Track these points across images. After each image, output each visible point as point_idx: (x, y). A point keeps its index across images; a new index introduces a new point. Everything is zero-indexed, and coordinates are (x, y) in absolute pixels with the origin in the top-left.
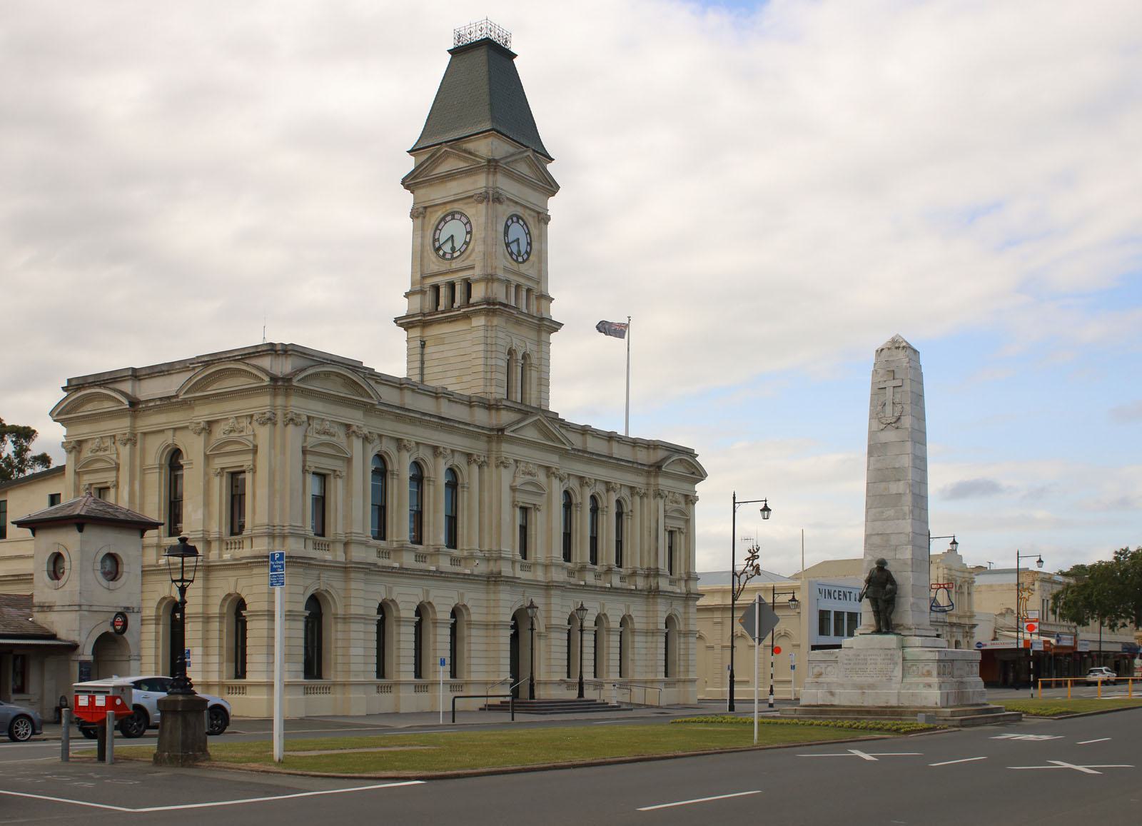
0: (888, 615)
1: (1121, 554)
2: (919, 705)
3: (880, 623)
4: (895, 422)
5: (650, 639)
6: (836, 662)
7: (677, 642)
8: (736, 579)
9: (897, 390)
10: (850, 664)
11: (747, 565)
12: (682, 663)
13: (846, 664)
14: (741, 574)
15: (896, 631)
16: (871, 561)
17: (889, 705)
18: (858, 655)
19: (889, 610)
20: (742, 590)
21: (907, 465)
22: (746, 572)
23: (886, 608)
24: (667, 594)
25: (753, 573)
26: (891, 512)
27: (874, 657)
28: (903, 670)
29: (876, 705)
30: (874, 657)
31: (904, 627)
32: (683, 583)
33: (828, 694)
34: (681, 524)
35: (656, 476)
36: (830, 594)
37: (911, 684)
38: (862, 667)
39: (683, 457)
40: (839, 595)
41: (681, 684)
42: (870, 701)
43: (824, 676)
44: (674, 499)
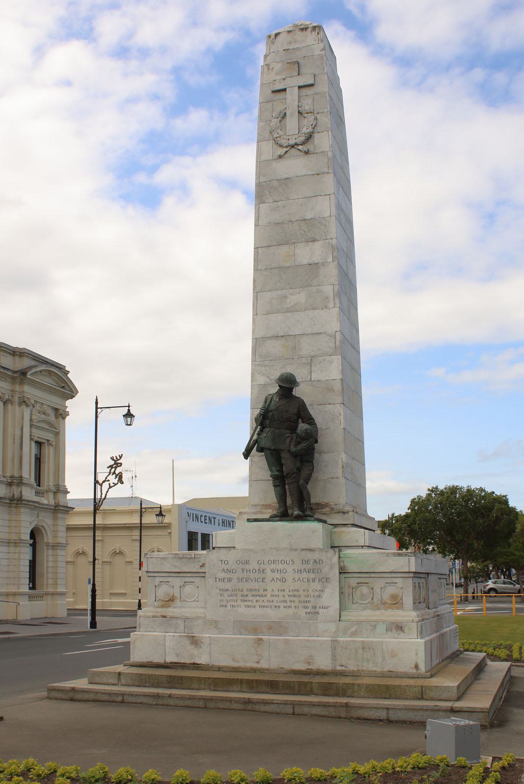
0: (301, 482)
1: (432, 491)
2: (379, 669)
3: (285, 502)
4: (303, 144)
5: (12, 549)
6: (202, 575)
7: (45, 554)
8: (98, 487)
9: (304, 91)
10: (230, 580)
11: (110, 473)
12: (50, 575)
13: (223, 580)
14: (104, 482)
15: (316, 516)
16: (265, 386)
17: (313, 667)
18: (247, 562)
19: (304, 473)
20: (105, 499)
21: (327, 214)
22: (109, 481)
23: (299, 470)
24: (31, 503)
25: (116, 481)
26: (300, 297)
27: (280, 566)
28: (341, 593)
29: (288, 666)
30: (280, 566)
31: (332, 509)
32: (51, 495)
33: (187, 642)
34: (50, 436)
35: (22, 383)
36: (197, 517)
37: (359, 623)
38: (255, 585)
39: (52, 370)
40: (205, 519)
41: (49, 597)
42: (275, 657)
43: (178, 603)
44: (42, 410)
